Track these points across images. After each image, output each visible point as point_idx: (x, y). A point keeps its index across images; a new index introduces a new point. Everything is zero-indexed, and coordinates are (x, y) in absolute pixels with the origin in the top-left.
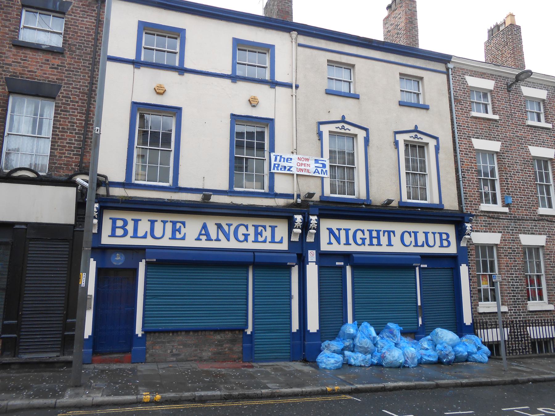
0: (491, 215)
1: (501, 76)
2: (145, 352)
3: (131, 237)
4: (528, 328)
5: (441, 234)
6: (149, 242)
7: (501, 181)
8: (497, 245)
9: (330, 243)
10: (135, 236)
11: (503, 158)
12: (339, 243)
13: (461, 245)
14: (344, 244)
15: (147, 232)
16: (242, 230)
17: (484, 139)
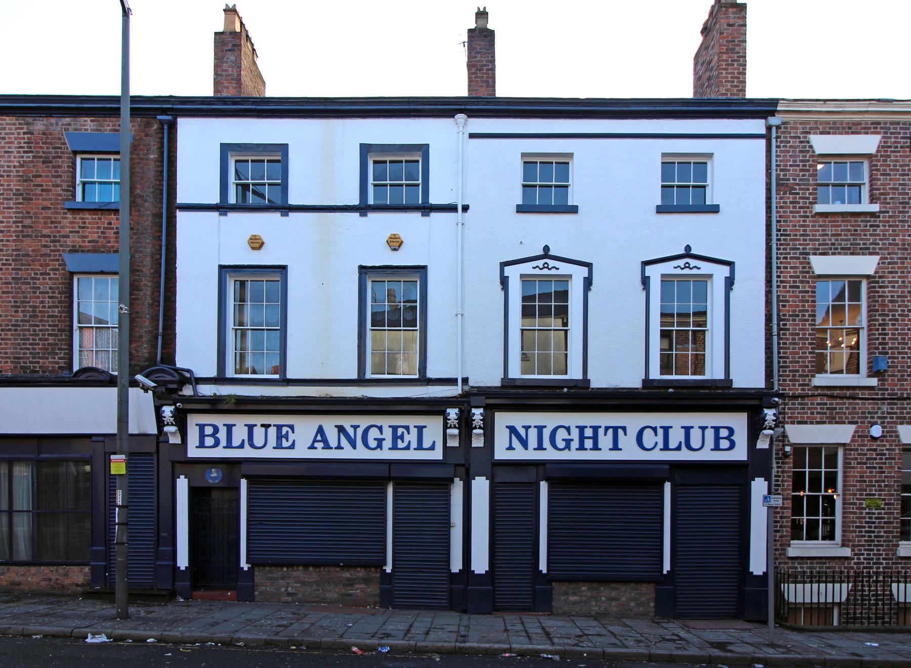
0: (836, 393)
1: (898, 123)
2: (253, 589)
3: (661, 450)
4: (894, 585)
5: (717, 429)
6: (248, 453)
7: (870, 330)
8: (844, 445)
9: (510, 448)
10: (229, 445)
11: (880, 287)
12: (526, 448)
13: (758, 447)
14: (535, 449)
15: (243, 441)
16: (374, 433)
17: (839, 254)
